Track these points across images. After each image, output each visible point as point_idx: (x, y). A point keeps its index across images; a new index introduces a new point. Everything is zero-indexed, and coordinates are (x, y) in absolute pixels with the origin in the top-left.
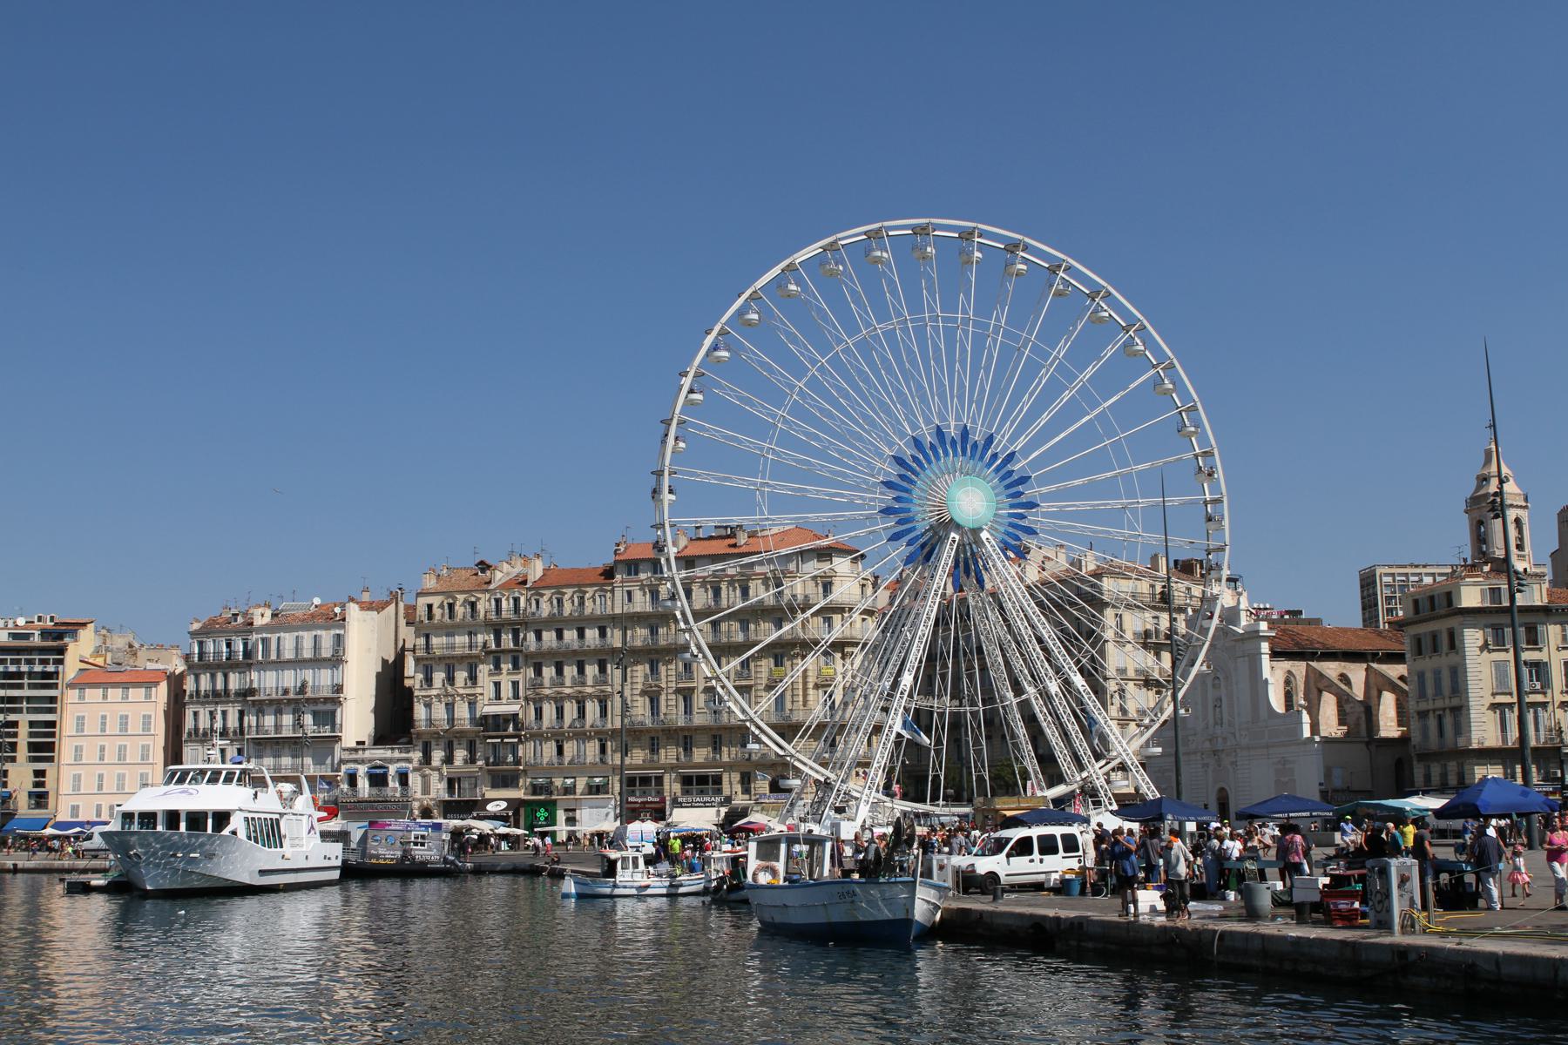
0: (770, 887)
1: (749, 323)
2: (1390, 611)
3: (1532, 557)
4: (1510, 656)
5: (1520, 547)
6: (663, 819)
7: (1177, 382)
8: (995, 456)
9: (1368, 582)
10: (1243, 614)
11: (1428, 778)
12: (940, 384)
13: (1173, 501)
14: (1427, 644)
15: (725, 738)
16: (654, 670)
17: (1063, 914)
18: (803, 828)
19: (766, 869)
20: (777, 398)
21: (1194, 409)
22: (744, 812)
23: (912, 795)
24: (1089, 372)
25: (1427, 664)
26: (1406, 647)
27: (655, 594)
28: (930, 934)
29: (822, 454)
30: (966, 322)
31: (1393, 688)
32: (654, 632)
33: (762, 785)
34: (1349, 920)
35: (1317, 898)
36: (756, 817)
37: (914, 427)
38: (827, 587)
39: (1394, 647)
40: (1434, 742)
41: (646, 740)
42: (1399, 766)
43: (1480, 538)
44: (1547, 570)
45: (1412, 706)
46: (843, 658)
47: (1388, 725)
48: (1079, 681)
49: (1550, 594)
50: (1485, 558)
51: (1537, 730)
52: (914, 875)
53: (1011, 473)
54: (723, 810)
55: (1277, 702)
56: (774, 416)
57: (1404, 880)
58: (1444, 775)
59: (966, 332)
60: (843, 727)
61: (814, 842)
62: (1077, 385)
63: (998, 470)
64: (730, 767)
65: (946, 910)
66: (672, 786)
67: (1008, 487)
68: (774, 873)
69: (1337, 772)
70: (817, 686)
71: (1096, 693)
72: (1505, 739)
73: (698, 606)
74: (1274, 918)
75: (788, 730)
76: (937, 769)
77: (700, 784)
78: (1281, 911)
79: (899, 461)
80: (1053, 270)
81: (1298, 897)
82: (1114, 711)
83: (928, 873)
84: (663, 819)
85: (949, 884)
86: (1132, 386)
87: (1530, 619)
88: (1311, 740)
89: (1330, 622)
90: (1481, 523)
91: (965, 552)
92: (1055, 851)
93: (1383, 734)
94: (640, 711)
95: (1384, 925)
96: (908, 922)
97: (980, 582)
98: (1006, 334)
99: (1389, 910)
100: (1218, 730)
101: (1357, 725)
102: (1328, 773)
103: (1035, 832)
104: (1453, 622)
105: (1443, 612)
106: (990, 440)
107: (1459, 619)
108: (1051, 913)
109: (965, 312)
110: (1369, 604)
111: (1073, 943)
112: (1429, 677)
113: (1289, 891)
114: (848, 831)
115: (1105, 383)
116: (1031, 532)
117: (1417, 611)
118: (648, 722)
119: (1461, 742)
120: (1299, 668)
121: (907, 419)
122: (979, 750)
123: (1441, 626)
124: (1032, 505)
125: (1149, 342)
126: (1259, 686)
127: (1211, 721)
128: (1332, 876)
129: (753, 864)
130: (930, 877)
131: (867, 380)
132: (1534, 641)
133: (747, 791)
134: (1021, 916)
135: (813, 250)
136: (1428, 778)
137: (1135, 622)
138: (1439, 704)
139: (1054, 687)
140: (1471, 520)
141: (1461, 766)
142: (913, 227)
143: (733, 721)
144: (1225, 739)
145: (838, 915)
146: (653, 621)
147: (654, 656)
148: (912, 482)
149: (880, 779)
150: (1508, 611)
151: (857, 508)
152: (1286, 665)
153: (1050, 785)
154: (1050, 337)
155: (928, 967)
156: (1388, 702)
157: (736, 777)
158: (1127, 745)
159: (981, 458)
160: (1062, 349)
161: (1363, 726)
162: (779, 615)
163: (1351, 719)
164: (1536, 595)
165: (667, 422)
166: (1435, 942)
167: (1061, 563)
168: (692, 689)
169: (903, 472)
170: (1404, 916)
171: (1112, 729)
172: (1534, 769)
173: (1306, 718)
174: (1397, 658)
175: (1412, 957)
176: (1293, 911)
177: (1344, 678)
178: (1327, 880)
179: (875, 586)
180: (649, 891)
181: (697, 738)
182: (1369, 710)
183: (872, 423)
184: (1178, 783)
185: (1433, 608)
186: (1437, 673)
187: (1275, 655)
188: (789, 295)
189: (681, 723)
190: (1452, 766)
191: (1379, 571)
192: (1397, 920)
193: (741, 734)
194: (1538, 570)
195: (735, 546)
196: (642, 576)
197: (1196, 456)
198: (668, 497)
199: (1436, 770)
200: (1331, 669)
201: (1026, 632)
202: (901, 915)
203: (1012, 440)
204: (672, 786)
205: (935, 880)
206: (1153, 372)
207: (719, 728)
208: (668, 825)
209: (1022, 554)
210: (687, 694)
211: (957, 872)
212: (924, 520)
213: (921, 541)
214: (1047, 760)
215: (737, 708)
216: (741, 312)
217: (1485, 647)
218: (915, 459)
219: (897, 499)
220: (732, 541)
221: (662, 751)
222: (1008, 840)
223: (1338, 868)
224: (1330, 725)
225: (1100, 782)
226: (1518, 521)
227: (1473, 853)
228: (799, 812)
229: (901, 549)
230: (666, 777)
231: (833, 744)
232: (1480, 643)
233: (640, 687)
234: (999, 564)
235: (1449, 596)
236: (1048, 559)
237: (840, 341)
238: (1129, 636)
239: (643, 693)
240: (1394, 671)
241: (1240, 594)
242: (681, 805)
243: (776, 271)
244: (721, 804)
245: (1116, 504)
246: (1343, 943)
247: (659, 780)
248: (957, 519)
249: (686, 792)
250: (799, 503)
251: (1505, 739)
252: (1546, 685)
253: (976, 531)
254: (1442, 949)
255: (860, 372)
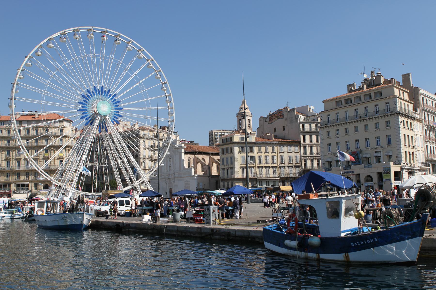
0: (41, 216)
1: (39, 55)
2: (216, 142)
3: (252, 129)
4: (245, 155)
5: (249, 127)
6: (11, 197)
7: (161, 75)
8: (111, 95)
9: (211, 134)
10: (178, 142)
11: (224, 186)
12: (95, 74)
13: (160, 108)
14: (225, 151)
15: (30, 174)
16: (8, 153)
17: (125, 222)
18: (52, 199)
19: (40, 210)
20: (47, 77)
21: (166, 83)
22: (35, 195)
23: (85, 190)
24: (137, 72)
25: (225, 156)
26: (220, 152)
27: (9, 131)
28: (87, 228)
29: (60, 94)
30: (103, 57)
31: (216, 162)
32: (9, 142)
33: (41, 187)
34: (200, 222)
35: (192, 216)
36: (39, 196)
37: (88, 86)
38: (62, 130)
39: (217, 151)
40: (226, 177)
41: (6, 174)
42: (216, 182)
43: (240, 124)
44: (256, 133)
45: (221, 167)
46: (66, 151)
47: (214, 172)
48: (132, 159)
49: (256, 139)
50: (241, 129)
51: (251, 174)
52: (84, 212)
53: (115, 100)
54: (29, 194)
55: (186, 165)
56: (46, 82)
57: (214, 211)
58: (228, 185)
59: (103, 60)
60: (65, 170)
61: (54, 203)
62: (134, 75)
63: (111, 99)
64: (31, 182)
65: (92, 221)
66: (13, 187)
67: (114, 104)
68: (43, 211)
69: (201, 184)
70: (58, 159)
71: (137, 162)
72: (243, 176)
73: (22, 135)
74: (181, 222)
75: (50, 171)
76: (95, 183)
77: (22, 187)
78: (183, 220)
79: (83, 96)
80: (128, 42)
81: (187, 216)
82: (142, 167)
83: (88, 211)
84: (11, 197)
85: (94, 214)
86: (149, 76)
87: (251, 145)
88: (194, 176)
89: (201, 145)
90: (240, 120)
91: (102, 122)
92: (124, 205)
93: (213, 174)
94: (4, 165)
95: (208, 223)
96: (82, 225)
97: (106, 130)
98: (114, 61)
99: (210, 219)
100: (170, 173)
101: (207, 172)
102: (198, 185)
103: (118, 200)
104: (232, 145)
105: (229, 142)
106: (109, 90)
107: (234, 144)
108: (121, 221)
109: (102, 54)
110: (211, 140)
111: (127, 229)
112: (225, 159)
113: (185, 215)
114: (67, 199)
115: (141, 75)
116: (121, 116)
117: (223, 142)
118: (6, 169)
119: (232, 177)
120: (192, 156)
121: (85, 84)
122: (107, 179)
123: (229, 146)
124: (121, 109)
125: (154, 64)
126: (181, 161)
127: (168, 170)
128: (196, 211)
129: (36, 209)
130: (88, 212)
131: (74, 72)
132: (251, 151)
133: (36, 189)
134: (113, 222)
135: (58, 34)
136: (224, 186)
137: (149, 143)
138: (227, 167)
139: (125, 160)
140: (238, 119)
141: (232, 183)
142: (88, 29)
143: (32, 169)
144: (172, 175)
145: (61, 223)
146: (9, 139)
147: (8, 149)
148: (87, 102)
149: (75, 185)
150: (245, 143)
151: (71, 109)
152: (188, 156)
153: (124, 187)
154: (126, 62)
155: (86, 235)
156: (215, 166)
157: (33, 185)
158: (145, 176)
159: (107, 96)
160: (130, 65)
161: (208, 172)
162: (47, 138)
163: (205, 170)
164: (252, 139)
165: (14, 84)
166: (220, 227)
167: (129, 126)
168: (20, 159)
169: (84, 99)
170: (213, 221)
171: (142, 173)
172: (250, 184)
173: (193, 170)
174: (217, 154)
175: (215, 231)
176: (186, 220)
177: (204, 159)
178: (195, 212)
179: (76, 131)
180: (5, 218)
181: (21, 173)
182: (210, 168)
183: (75, 85)
184: (159, 187)
185: (227, 142)
186: (227, 158)
187: (186, 153)
188: (50, 47)
189: (17, 169)
190: (230, 183)
191: (214, 131)
192: (212, 222)
193: (36, 173)
194: (254, 133)
195: (34, 118)
196: (5, 126)
197: (166, 96)
198: (14, 106)
199: (226, 184)
200: (200, 157)
201: (118, 145)
202: (80, 223)
203: (115, 91)
204: (13, 187)
205: (90, 213)
206: (155, 72)
207: (28, 171)
208: (12, 199)
209: (118, 123)
210: (18, 161)
211: (96, 211)
212: (90, 113)
213: (90, 119)
214: (123, 180)
215: (34, 166)
216: (36, 52)
217: (239, 152)
218: (88, 95)
219: (82, 107)
220: (33, 116)
221: (11, 177)
222: (110, 202)
223: (198, 209)
224: (200, 172)
225: (137, 186)
226: (249, 120)
227: (116, 238)
228: (53, 193)
229: (83, 121)
230: (12, 185)
231: (62, 175)
232: (238, 151)
233: (4, 158)
234: (111, 126)
235: (231, 138)
236: (125, 125)
237: (66, 61)
238: (147, 147)
239: (5, 160)
240: (216, 158)
241: (177, 136)
242: (16, 193)
243: (47, 40)
244: (28, 193)
245: (144, 109)
246: (198, 228)
247: (10, 186)
248: (100, 113)
249: (18, 189)
250: (54, 108)
251: (243, 176)
252: (254, 162)
253: (105, 116)
254: (222, 229)
255: (72, 70)
